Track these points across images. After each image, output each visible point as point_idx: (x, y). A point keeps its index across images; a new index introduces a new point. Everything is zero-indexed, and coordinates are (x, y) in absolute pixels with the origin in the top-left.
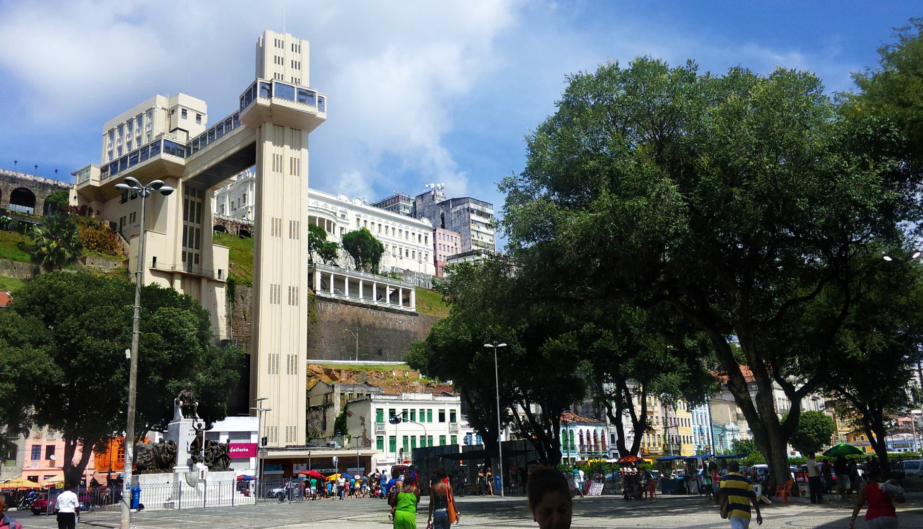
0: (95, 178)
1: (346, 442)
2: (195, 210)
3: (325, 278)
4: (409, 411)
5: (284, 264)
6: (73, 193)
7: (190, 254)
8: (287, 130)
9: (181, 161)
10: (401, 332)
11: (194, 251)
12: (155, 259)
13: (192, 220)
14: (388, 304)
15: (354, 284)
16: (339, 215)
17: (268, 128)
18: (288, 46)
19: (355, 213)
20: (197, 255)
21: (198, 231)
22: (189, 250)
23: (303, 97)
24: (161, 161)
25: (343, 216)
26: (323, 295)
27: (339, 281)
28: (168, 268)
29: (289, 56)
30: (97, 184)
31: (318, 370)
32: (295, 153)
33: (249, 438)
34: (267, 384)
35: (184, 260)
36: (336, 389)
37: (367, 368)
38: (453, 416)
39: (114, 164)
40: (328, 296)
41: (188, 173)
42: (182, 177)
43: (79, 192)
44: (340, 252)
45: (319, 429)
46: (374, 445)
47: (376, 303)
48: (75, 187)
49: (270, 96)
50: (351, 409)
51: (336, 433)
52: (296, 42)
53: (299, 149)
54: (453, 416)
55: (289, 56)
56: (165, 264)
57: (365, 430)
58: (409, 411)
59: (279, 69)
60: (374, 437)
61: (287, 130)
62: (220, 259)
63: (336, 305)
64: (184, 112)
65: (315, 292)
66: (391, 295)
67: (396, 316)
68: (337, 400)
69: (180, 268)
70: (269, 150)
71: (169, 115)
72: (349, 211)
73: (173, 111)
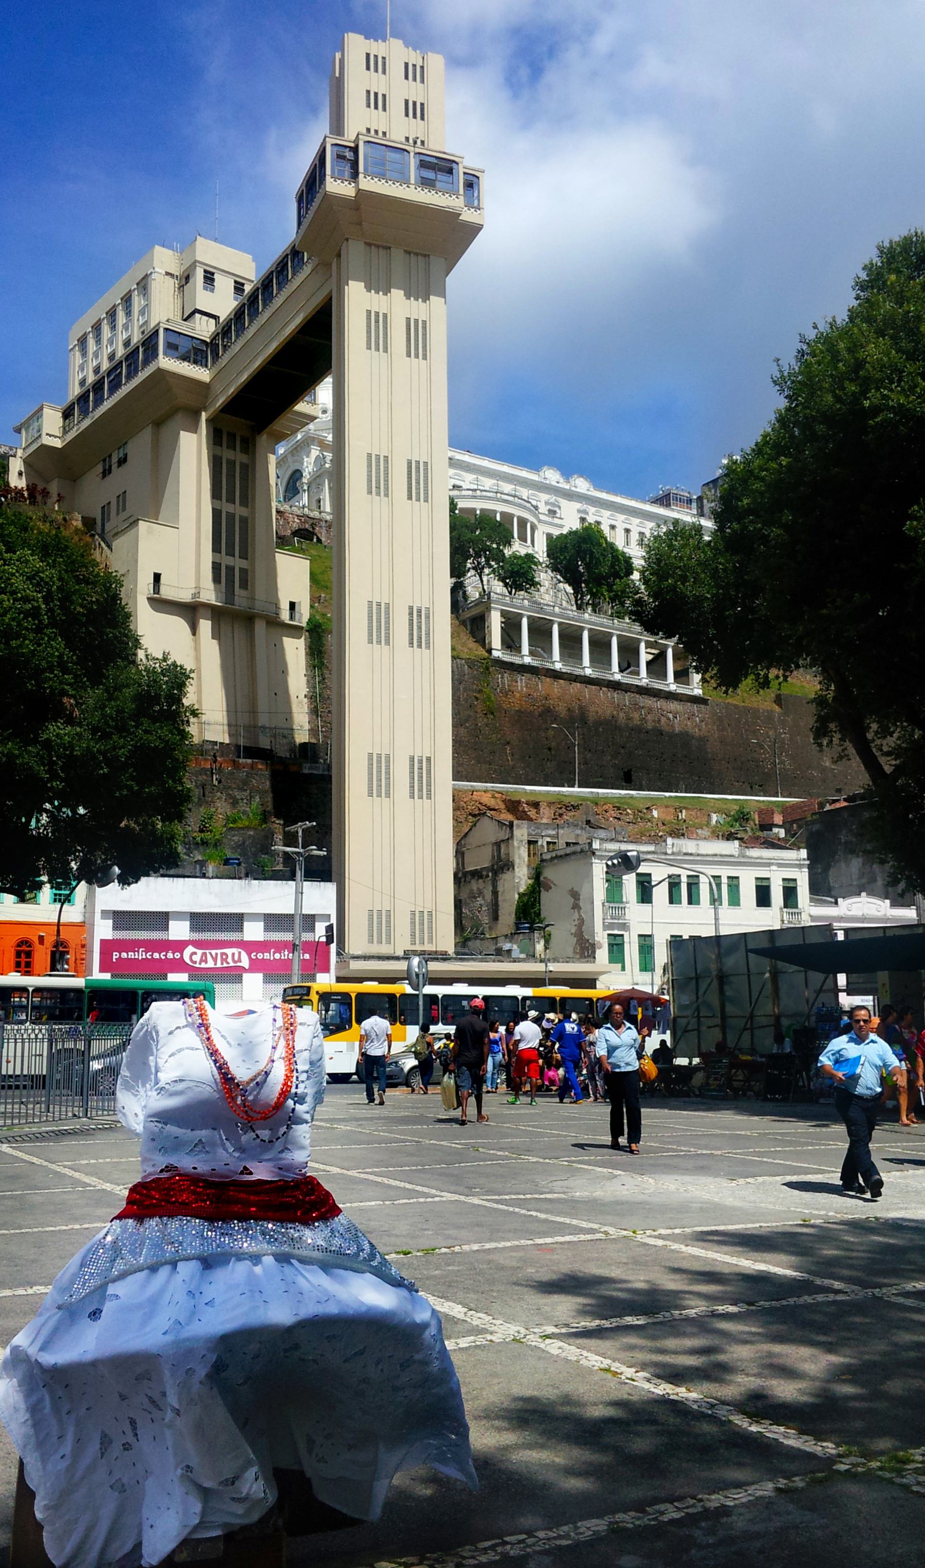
0: (52, 430)
1: (540, 947)
2: (234, 480)
3: (511, 626)
4: (684, 879)
5: (396, 562)
6: (16, 465)
7: (230, 569)
8: (398, 255)
9: (202, 374)
10: (672, 736)
11: (238, 563)
12: (157, 577)
13: (231, 500)
14: (643, 678)
15: (571, 640)
16: (543, 509)
17: (355, 252)
18: (395, 69)
19: (578, 505)
20: (243, 571)
21: (244, 521)
22: (227, 560)
23: (430, 175)
24: (160, 372)
25: (552, 513)
26: (507, 658)
27: (540, 631)
28: (185, 596)
29: (399, 90)
30: (58, 444)
31: (492, 803)
32: (417, 309)
33: (166, 928)
34: (364, 818)
35: (216, 579)
36: (517, 832)
37: (596, 802)
38: (790, 893)
39: (83, 399)
40: (517, 660)
41: (216, 398)
42: (205, 409)
43: (26, 462)
44: (545, 577)
45: (485, 919)
46: (602, 954)
47: (618, 677)
48: (20, 453)
49: (355, 175)
50: (549, 873)
51: (518, 926)
52: (414, 57)
53: (426, 299)
54: (790, 893)
55: (399, 90)
56: (179, 588)
57: (582, 921)
58: (684, 879)
59: (376, 120)
60: (601, 937)
61: (398, 255)
62: (292, 578)
63: (534, 679)
64: (209, 278)
65: (490, 651)
66: (649, 663)
67: (661, 704)
68: (521, 856)
69: (209, 595)
70: (358, 301)
71: (181, 287)
72: (563, 502)
73: (187, 278)
